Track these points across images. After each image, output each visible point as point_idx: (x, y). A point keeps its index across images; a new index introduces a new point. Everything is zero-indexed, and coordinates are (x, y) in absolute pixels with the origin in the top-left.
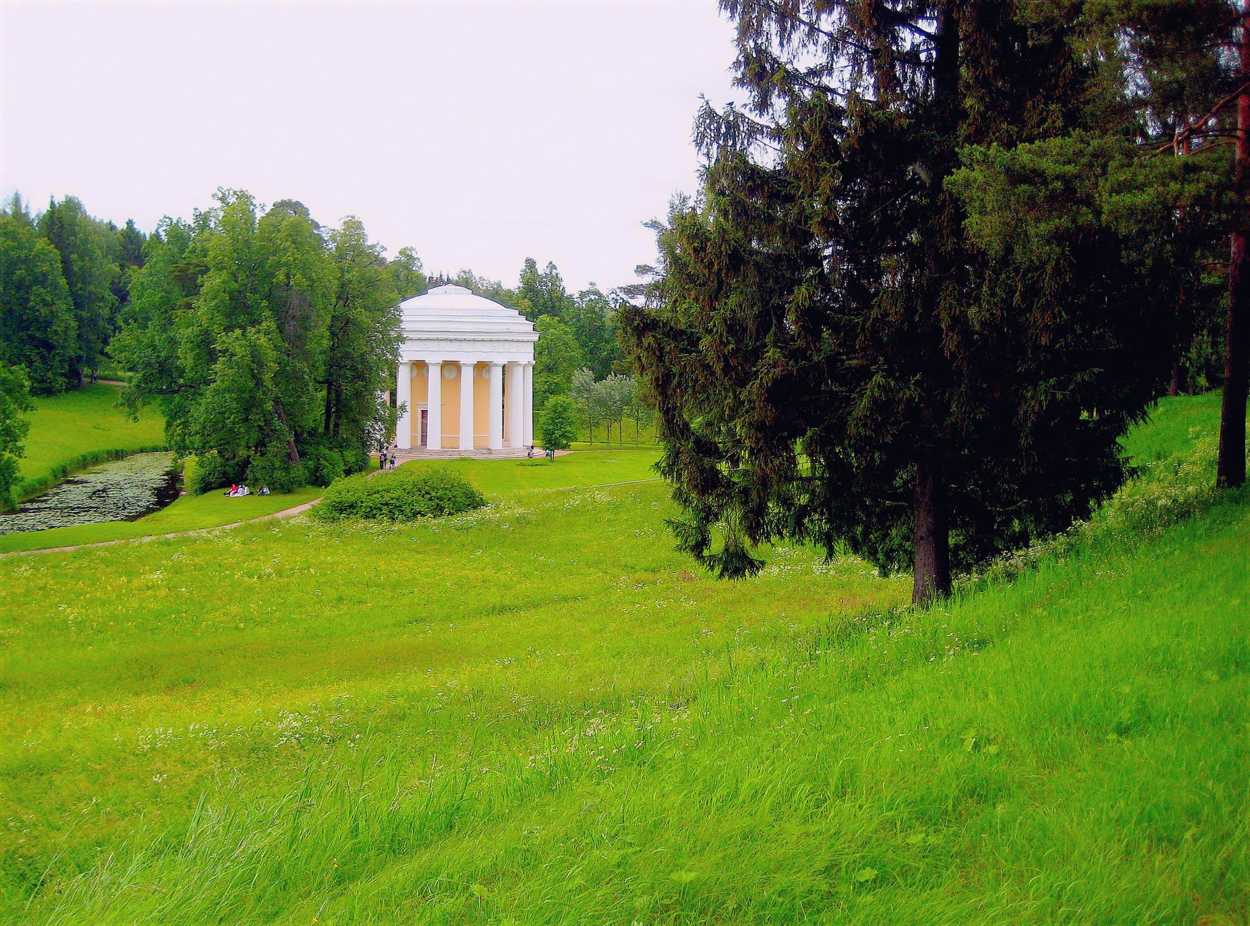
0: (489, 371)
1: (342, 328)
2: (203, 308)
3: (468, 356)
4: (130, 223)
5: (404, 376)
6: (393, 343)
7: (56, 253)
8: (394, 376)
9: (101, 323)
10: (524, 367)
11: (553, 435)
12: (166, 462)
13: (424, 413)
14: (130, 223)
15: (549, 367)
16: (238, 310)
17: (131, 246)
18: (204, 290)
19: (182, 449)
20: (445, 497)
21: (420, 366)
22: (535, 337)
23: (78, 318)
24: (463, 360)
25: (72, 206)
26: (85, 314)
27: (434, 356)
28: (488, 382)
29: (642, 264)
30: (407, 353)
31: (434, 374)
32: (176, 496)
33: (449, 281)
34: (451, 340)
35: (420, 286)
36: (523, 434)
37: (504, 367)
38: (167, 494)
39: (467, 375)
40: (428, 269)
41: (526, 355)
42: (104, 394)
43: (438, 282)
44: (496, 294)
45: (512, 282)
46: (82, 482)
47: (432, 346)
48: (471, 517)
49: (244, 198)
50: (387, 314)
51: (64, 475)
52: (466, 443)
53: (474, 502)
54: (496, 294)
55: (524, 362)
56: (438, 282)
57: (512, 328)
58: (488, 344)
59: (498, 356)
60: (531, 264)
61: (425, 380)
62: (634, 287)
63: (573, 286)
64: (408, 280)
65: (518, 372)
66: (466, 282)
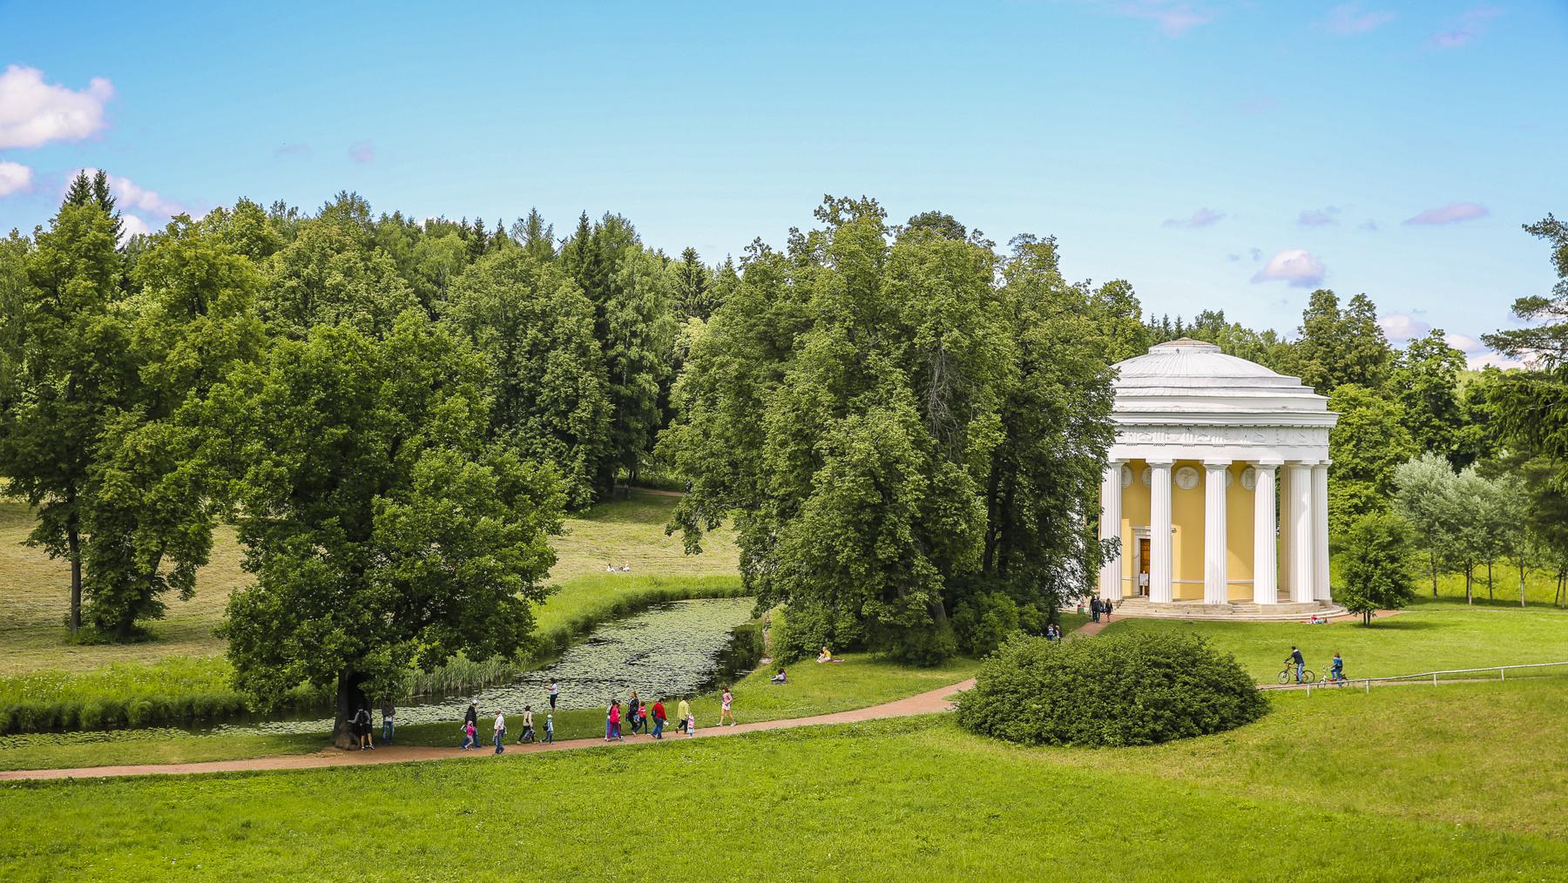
0: (1253, 477)
1: (1025, 416)
2: (802, 378)
3: (1217, 452)
4: (690, 256)
6: (1097, 431)
7: (586, 305)
8: (1097, 480)
9: (646, 404)
10: (1314, 469)
11: (1373, 583)
12: (739, 613)
13: (1145, 543)
14: (690, 256)
15: (1359, 469)
16: (852, 383)
18: (802, 355)
19: (766, 597)
20: (1186, 692)
21: (1137, 470)
22: (1332, 422)
23: (616, 398)
26: (624, 390)
27: (1160, 450)
28: (1251, 493)
31: (1160, 482)
32: (750, 665)
33: (1180, 334)
34: (1204, 427)
35: (1141, 341)
36: (1313, 576)
37: (1278, 470)
38: (737, 658)
39: (1215, 484)
40: (1152, 309)
41: (1316, 451)
43: (1168, 334)
44: (1260, 350)
45: (1289, 327)
46: (613, 641)
48: (1251, 736)
49: (868, 211)
50: (1097, 394)
51: (585, 628)
52: (1215, 592)
54: (1260, 350)
55: (1314, 461)
56: (1168, 334)
57: (1292, 407)
58: (1253, 433)
60: (1325, 301)
61: (1147, 489)
62: (1514, 335)
63: (1397, 329)
64: (1122, 326)
65: (1301, 481)
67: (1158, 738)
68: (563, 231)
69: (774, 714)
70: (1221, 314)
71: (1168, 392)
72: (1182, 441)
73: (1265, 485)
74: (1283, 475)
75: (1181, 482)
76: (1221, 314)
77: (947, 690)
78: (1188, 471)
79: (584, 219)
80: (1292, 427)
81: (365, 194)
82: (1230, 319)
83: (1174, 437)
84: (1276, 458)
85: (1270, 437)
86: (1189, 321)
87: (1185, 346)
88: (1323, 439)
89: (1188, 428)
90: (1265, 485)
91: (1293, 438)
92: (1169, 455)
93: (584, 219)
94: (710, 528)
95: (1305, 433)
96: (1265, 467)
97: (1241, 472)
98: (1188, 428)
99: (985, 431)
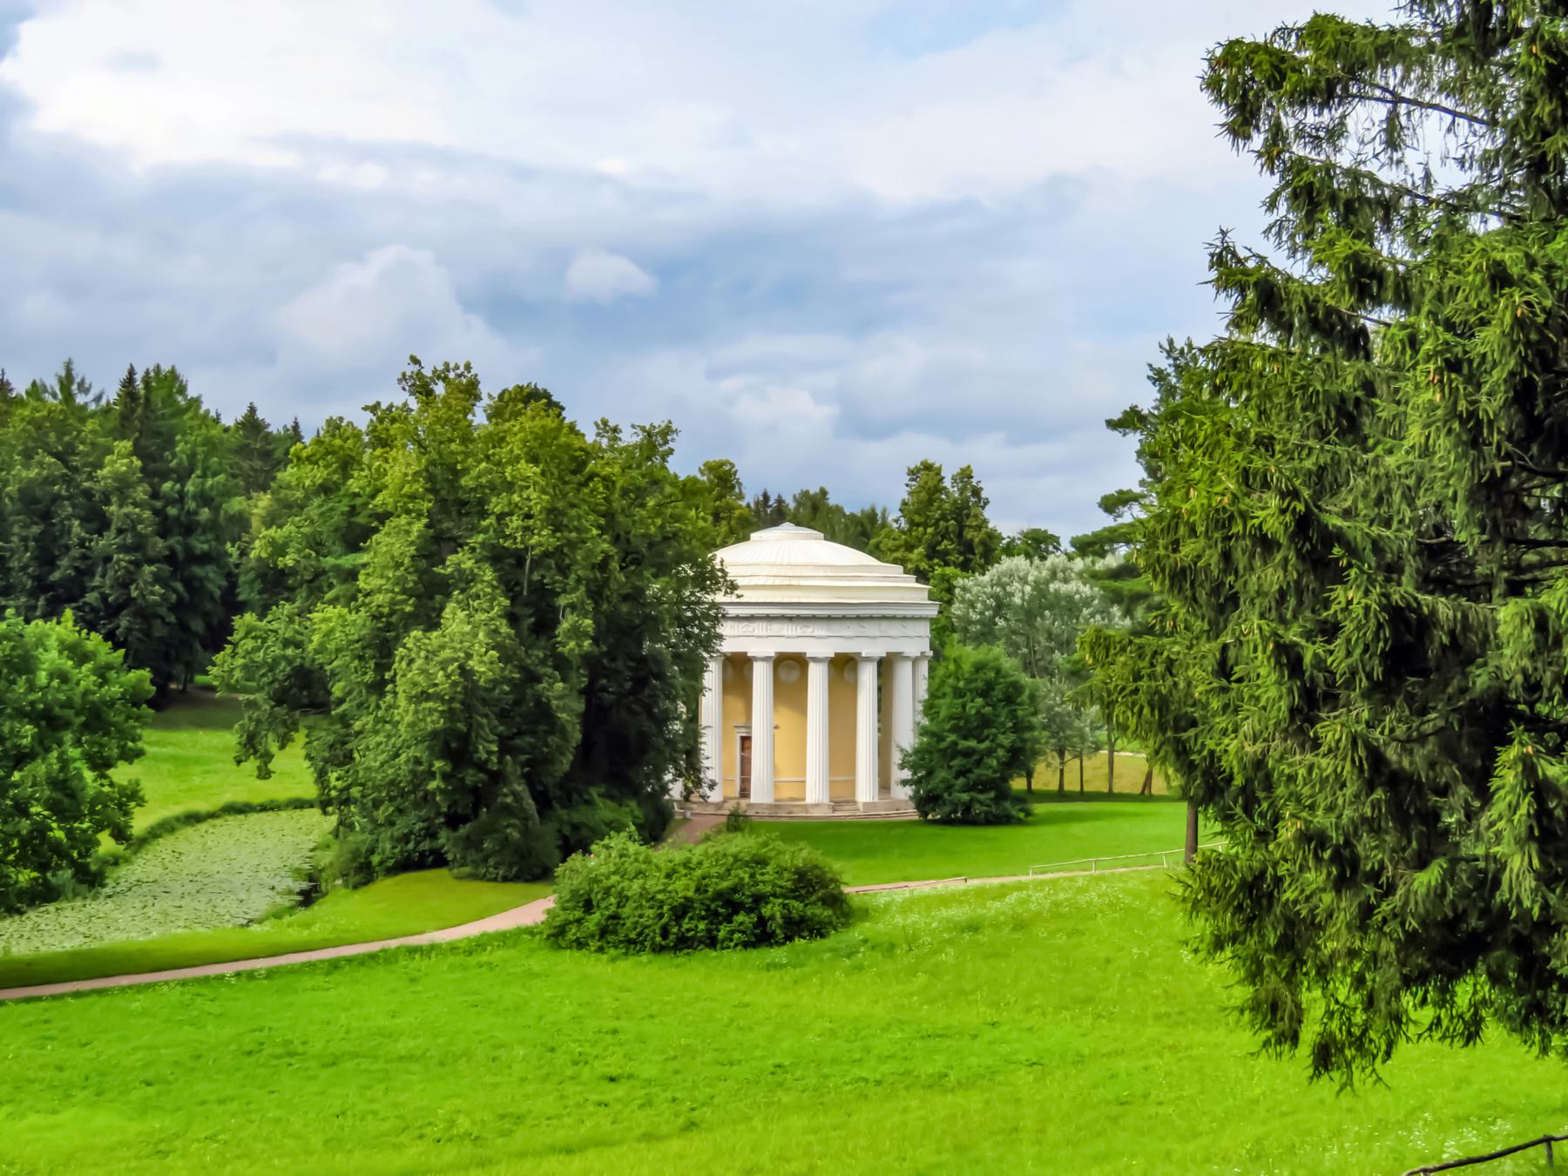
0: (855, 670)
5: (712, 678)
10: (915, 661)
13: (746, 741)
17: (259, 449)
21: (738, 667)
22: (933, 612)
24: (753, 649)
25: (170, 381)
29: (1111, 490)
30: (733, 639)
35: (742, 527)
39: (817, 677)
41: (915, 642)
42: (646, 673)
45: (890, 496)
47: (759, 628)
52: (815, 793)
53: (1112, 425)
54: (861, 532)
56: (771, 514)
58: (824, 624)
59: (870, 644)
64: (727, 506)
65: (904, 674)
66: (814, 512)
67: (684, 944)
68: (105, 386)
69: (958, 913)
70: (824, 493)
71: (770, 582)
72: (784, 632)
73: (868, 677)
74: (886, 666)
75: (783, 675)
76: (824, 493)
77: (535, 908)
78: (790, 666)
79: (131, 372)
80: (894, 618)
81: (184, 374)
82: (832, 500)
83: (776, 628)
84: (879, 650)
85: (871, 629)
86: (853, 507)
87: (786, 530)
88: (924, 630)
89: (790, 619)
90: (868, 677)
91: (895, 629)
92: (771, 649)
93: (131, 372)
94: (282, 747)
95: (907, 624)
96: (868, 659)
97: (843, 666)
98: (790, 619)
99: (575, 629)
